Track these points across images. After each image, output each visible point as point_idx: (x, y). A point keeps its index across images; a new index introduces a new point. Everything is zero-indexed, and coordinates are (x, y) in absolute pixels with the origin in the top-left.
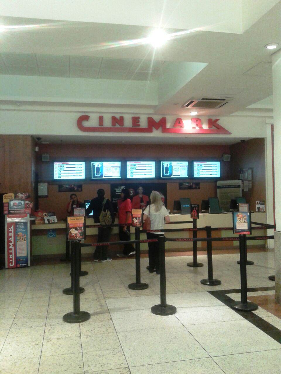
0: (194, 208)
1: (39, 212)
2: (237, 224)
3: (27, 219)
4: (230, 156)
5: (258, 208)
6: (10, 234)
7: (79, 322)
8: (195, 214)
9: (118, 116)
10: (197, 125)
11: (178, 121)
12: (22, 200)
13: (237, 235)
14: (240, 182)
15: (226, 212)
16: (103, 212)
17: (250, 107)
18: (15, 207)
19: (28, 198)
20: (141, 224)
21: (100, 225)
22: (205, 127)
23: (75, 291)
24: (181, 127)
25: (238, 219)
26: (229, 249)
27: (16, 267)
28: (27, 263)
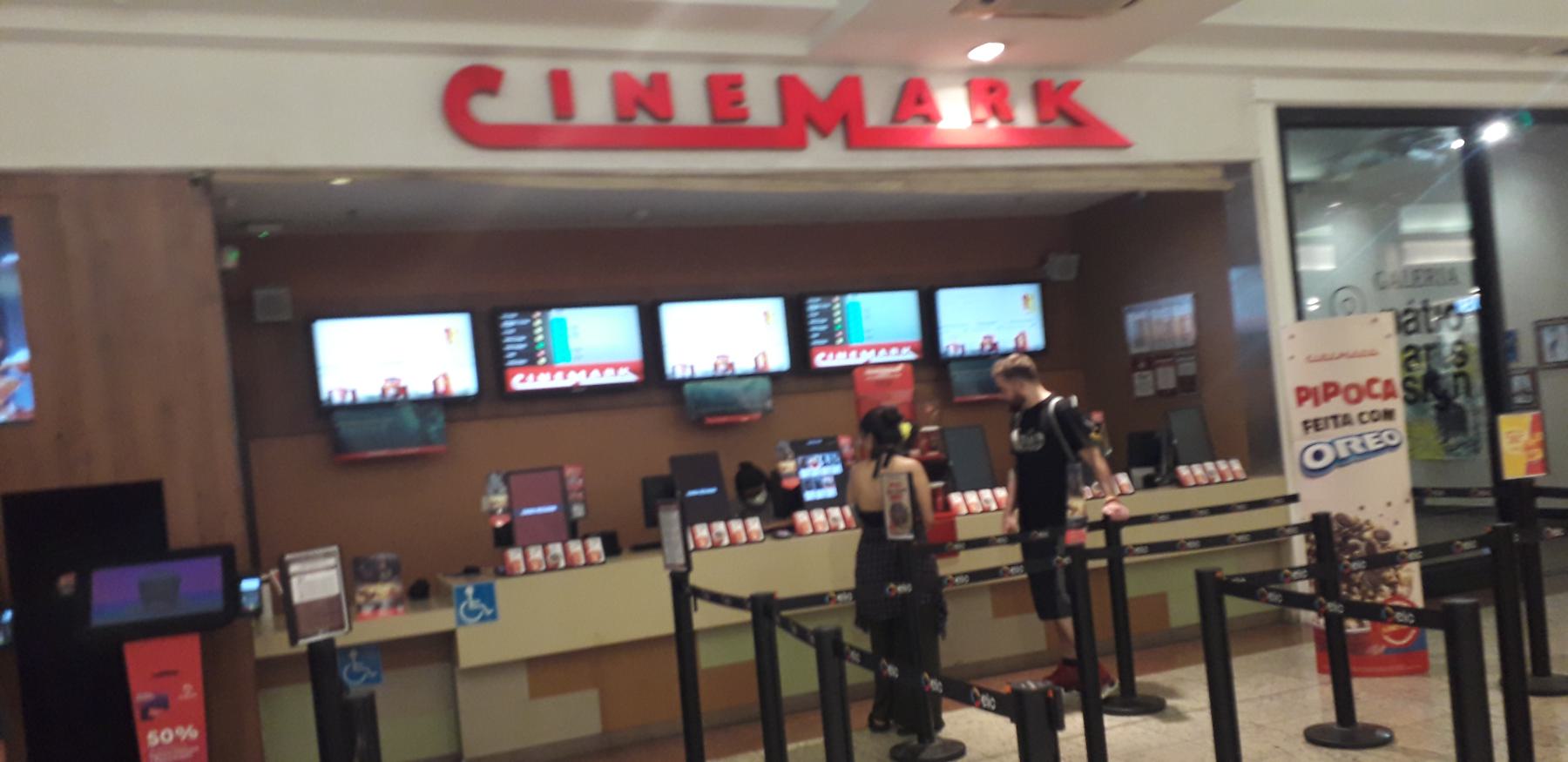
9: (640, 72)
22: (1025, 116)
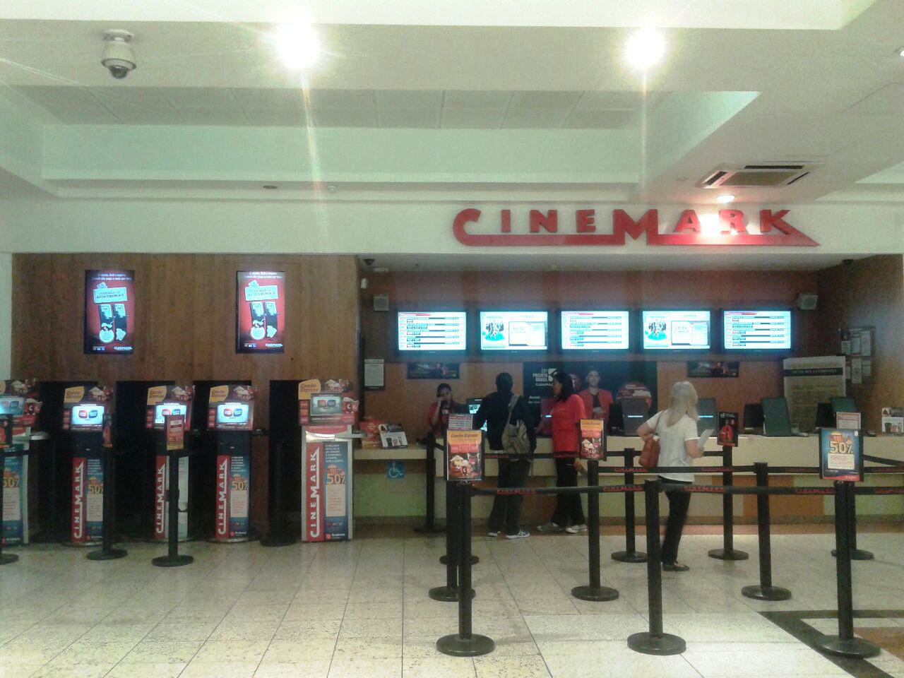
0: (727, 422)
1: (368, 421)
2: (829, 455)
3: (347, 436)
4: (815, 297)
5: (886, 424)
7: (471, 655)
8: (728, 436)
9: (544, 210)
10: (733, 225)
11: (687, 219)
12: (336, 395)
13: (829, 483)
14: (840, 361)
15: (805, 434)
16: (509, 427)
17: (866, 180)
18: (322, 410)
19: (347, 391)
20: (600, 454)
21: (501, 454)
22: (754, 229)
23: (458, 590)
24: (694, 230)
25: (832, 445)
26: (810, 522)
27: (323, 539)
28: (346, 532)
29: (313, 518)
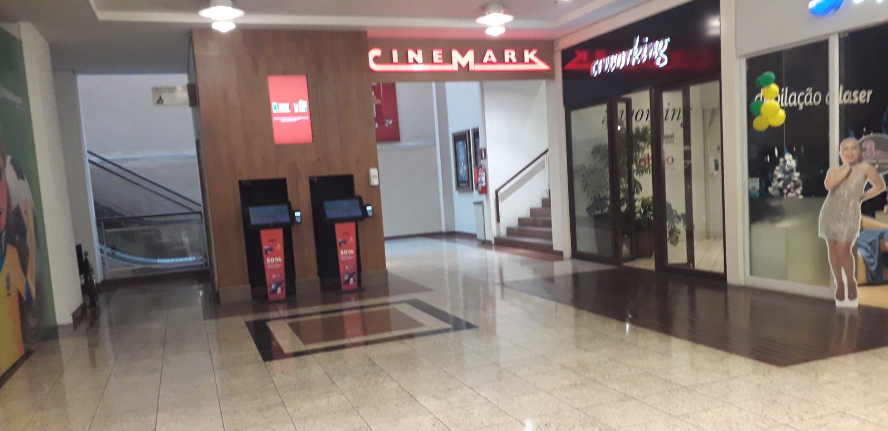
6: (513, 53)
29: (528, 55)
